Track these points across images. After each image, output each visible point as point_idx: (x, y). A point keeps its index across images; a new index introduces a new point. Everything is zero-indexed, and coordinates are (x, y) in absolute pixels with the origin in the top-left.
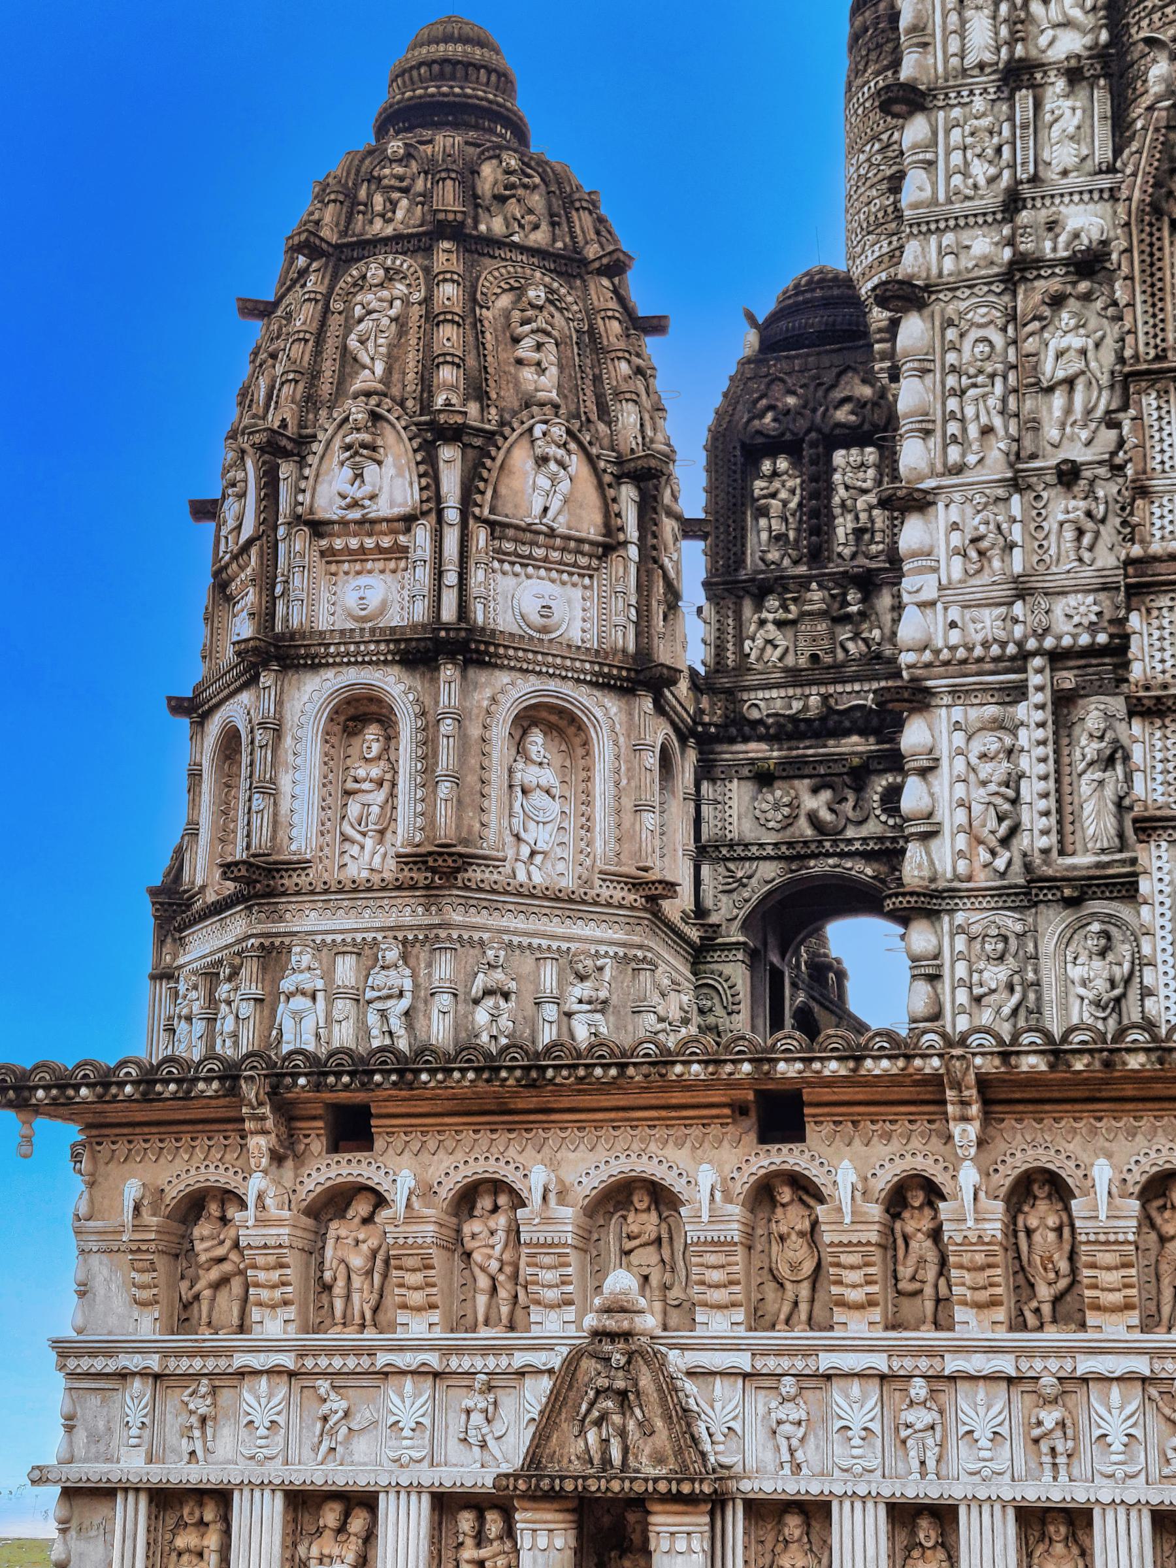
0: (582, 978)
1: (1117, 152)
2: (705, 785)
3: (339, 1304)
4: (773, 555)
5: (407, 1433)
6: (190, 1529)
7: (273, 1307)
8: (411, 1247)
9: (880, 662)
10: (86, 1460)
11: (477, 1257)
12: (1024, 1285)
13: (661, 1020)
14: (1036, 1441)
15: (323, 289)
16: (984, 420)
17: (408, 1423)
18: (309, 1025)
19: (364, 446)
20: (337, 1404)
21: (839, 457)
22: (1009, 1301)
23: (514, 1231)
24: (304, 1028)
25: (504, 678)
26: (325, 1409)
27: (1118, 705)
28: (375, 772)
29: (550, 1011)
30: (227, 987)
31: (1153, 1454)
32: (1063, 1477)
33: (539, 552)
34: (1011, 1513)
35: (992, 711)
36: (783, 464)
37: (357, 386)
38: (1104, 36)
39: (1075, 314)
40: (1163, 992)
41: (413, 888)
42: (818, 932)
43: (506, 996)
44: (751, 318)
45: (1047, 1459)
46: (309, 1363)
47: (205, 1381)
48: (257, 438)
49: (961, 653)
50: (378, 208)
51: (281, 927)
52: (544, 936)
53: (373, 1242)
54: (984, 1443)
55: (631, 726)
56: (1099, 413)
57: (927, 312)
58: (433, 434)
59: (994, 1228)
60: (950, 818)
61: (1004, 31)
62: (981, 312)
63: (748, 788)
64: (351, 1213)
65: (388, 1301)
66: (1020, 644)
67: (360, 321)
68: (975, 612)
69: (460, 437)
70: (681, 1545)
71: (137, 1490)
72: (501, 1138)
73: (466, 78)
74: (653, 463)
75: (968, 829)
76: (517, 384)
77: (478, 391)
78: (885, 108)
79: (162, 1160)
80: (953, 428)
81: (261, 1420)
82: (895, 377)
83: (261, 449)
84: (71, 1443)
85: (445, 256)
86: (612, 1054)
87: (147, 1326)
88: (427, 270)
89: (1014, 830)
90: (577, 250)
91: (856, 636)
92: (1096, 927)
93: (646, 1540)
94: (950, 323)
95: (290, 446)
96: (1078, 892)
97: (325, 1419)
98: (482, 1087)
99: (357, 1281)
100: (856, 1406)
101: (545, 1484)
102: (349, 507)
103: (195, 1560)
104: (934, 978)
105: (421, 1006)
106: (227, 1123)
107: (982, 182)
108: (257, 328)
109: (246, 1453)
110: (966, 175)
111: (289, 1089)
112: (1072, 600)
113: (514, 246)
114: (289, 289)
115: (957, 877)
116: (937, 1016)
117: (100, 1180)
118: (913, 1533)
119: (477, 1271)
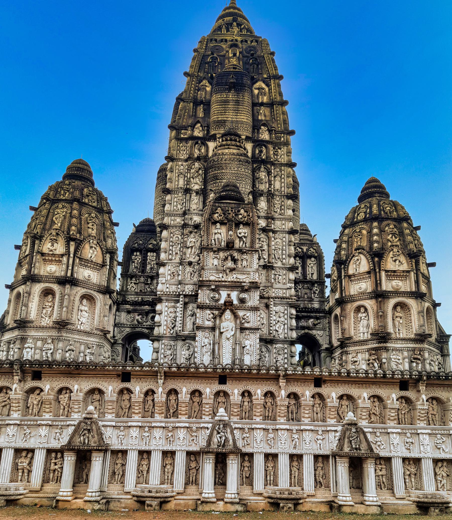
0: (89, 348)
1: (203, 208)
2: (117, 312)
3: (30, 411)
4: (135, 270)
5: (43, 437)
7: (16, 411)
9: (153, 293)
11: (61, 402)
12: (168, 410)
13: (104, 357)
14: (167, 439)
15: (49, 207)
16: (176, 251)
17: (43, 435)
18: (30, 354)
19: (54, 239)
20: (28, 431)
21: (149, 254)
22: (165, 413)
23: (70, 398)
24: (28, 355)
25: (79, 288)
26: (25, 432)
27: (195, 305)
28: (50, 304)
29: (82, 355)
30: (12, 345)
31: (188, 441)
32: (171, 445)
33: (89, 265)
34: (161, 452)
35: (173, 304)
36: (138, 254)
37: (54, 227)
38: (203, 187)
39: (194, 235)
40: (198, 358)
41: (56, 328)
42: (136, 342)
43: (73, 351)
44: (134, 225)
45: (169, 442)
46: (23, 423)
48: (31, 235)
49: (168, 293)
50: (62, 193)
51: (26, 334)
52: (82, 340)
53: (39, 399)
54: (158, 439)
55: (104, 300)
56: (196, 253)
57: (168, 230)
58: (69, 239)
59: (164, 400)
60: (163, 323)
61: (186, 182)
62: (178, 233)
63: (126, 314)
64: (35, 393)
65: (41, 410)
66: (179, 293)
67: (56, 215)
68: (172, 286)
69: (75, 240)
70: (98, 459)
72: (69, 379)
73: (83, 171)
74: (114, 251)
75: (166, 325)
76: (88, 231)
77: (79, 232)
78: (163, 192)
80: (170, 252)
81: (11, 434)
82: (161, 241)
83: (32, 237)
85: (75, 205)
86: (94, 364)
88: (71, 207)
89: (175, 326)
90: (102, 208)
91: (149, 287)
92: (187, 345)
93: (91, 458)
94: (172, 233)
95: (38, 237)
96: (185, 338)
97: (25, 434)
98: (66, 369)
99: (35, 406)
100: (134, 432)
101: (71, 447)
102: (50, 251)
104: (157, 352)
105: (55, 352)
106: (10, 373)
107: (179, 209)
108: (33, 213)
109: (7, 441)
110: (177, 207)
111: (24, 367)
112: (189, 286)
113: (89, 205)
114: (41, 206)
115: (163, 334)
116: (157, 359)
118: (143, 456)
119: (61, 405)
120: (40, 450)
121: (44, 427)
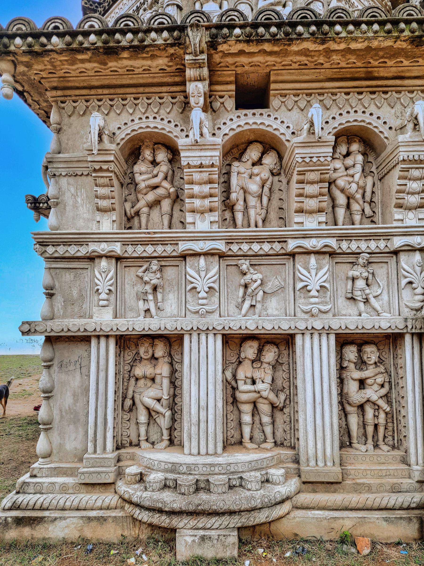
6: (144, 362)
8: (315, 164)
10: (64, 316)
17: (314, 286)
47: (155, 262)
71: (107, 337)
79: (112, 114)
81: (202, 285)
84: (52, 306)
87: (107, 224)
97: (246, 286)
99: (252, 201)
103: (149, 383)
117: (65, 128)
120: (316, 337)
121: (313, 260)
